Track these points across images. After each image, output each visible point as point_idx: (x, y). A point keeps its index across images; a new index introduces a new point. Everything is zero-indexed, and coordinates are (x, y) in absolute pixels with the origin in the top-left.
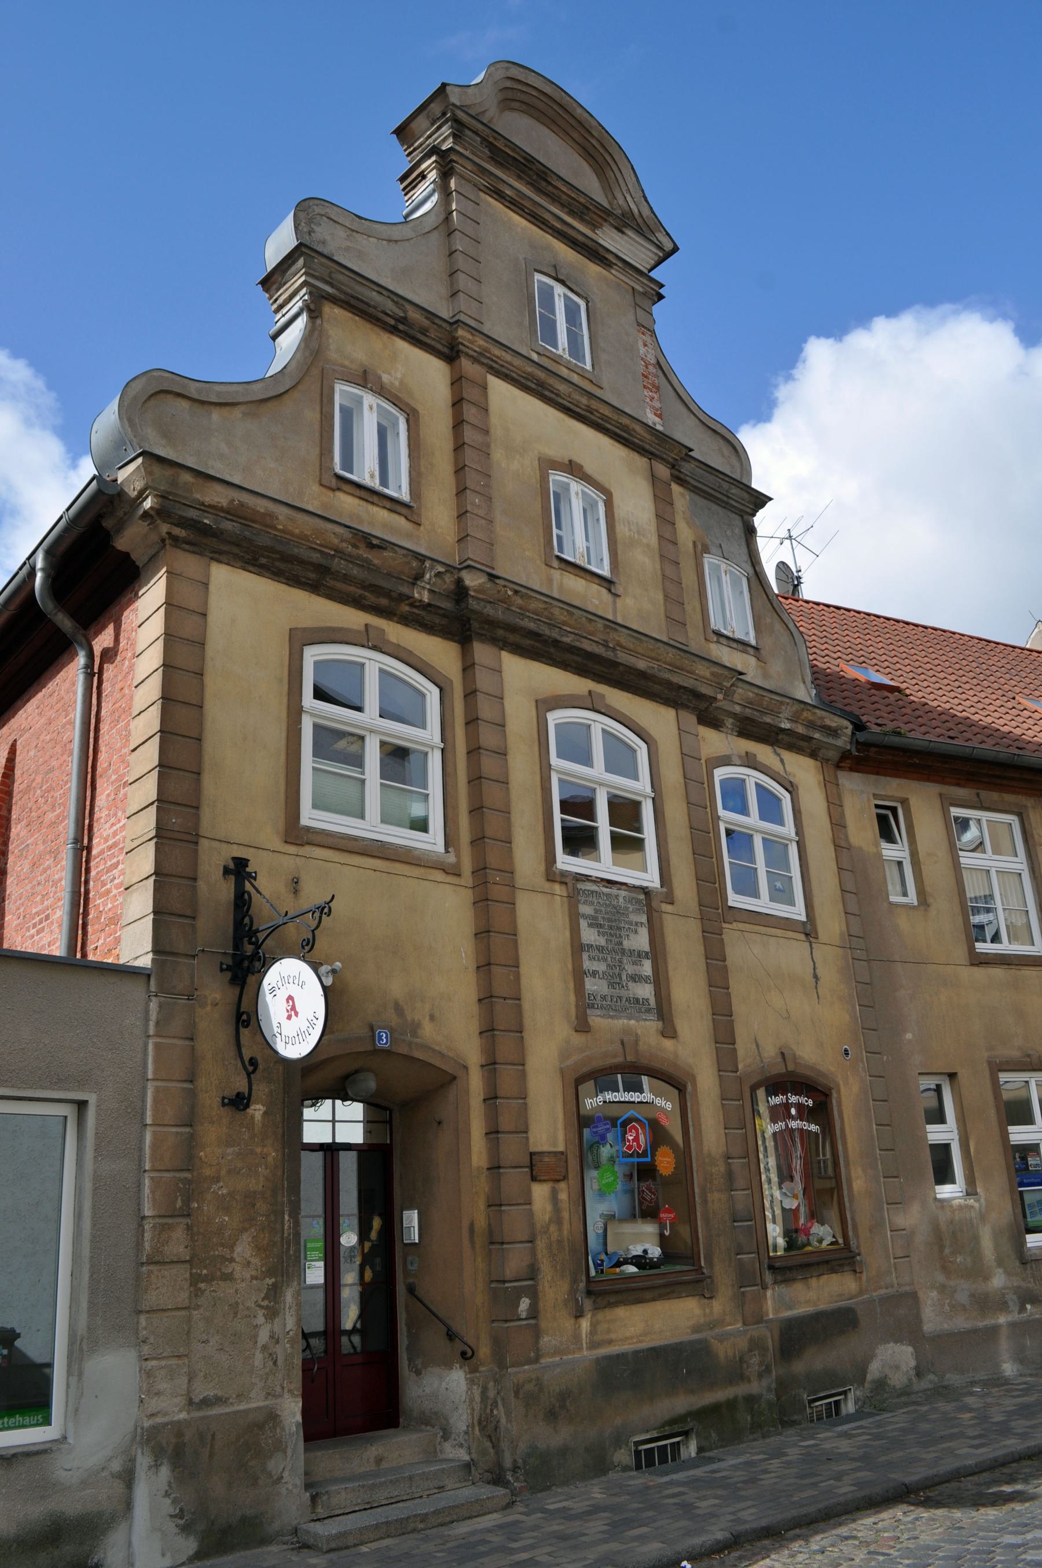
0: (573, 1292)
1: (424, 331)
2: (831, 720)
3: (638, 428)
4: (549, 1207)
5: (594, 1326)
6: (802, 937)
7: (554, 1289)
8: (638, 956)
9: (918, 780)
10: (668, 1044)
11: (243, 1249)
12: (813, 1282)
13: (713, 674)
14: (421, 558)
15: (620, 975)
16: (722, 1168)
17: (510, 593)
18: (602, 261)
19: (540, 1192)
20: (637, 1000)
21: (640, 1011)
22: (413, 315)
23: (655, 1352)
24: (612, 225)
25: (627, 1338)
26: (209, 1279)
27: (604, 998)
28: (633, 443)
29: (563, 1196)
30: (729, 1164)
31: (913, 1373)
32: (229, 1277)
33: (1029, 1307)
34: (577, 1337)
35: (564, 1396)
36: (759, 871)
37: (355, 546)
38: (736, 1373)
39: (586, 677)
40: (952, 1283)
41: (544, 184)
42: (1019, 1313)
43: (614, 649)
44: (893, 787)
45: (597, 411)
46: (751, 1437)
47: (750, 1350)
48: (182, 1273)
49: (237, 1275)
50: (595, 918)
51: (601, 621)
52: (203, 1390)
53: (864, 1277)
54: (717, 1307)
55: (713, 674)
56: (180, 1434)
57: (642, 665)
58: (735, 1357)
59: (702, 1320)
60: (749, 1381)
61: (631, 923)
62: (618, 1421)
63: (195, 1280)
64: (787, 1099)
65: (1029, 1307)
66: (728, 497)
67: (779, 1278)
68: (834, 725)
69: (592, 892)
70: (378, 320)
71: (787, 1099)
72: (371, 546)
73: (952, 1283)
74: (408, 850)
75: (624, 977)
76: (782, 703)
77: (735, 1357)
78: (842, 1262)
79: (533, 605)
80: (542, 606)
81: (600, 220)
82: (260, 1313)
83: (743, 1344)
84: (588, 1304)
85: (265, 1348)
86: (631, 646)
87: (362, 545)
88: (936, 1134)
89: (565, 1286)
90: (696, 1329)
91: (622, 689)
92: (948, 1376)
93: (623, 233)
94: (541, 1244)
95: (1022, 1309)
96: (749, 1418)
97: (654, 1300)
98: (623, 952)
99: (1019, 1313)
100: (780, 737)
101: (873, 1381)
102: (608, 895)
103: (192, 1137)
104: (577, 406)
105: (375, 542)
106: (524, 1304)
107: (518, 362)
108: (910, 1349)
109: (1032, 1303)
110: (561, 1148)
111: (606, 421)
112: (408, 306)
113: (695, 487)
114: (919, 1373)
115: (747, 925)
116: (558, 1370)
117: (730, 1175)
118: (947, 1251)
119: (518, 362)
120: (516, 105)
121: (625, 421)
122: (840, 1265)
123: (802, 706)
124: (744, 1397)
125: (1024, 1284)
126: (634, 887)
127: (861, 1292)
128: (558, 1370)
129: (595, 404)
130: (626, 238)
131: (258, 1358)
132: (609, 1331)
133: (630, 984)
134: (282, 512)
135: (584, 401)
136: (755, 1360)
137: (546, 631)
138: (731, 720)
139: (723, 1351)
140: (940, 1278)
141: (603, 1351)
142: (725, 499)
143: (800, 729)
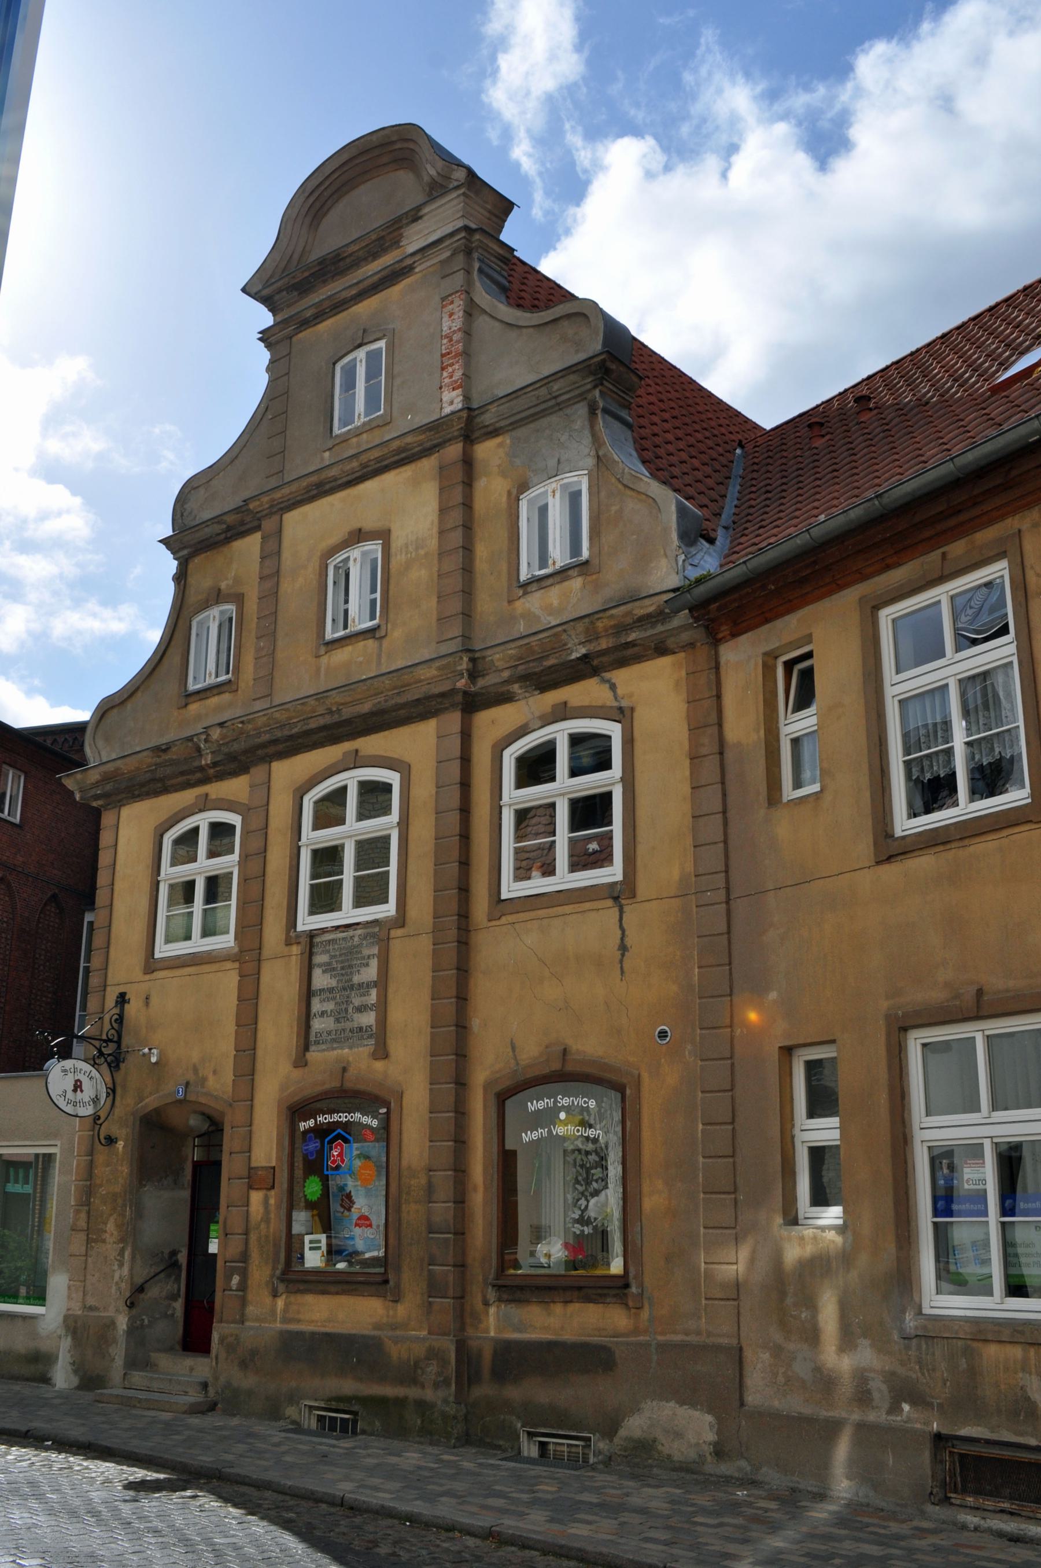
0: (272, 1276)
1: (242, 523)
2: (642, 608)
3: (409, 439)
4: (261, 1210)
5: (287, 1305)
6: (609, 903)
7: (260, 1272)
8: (364, 988)
9: (830, 593)
10: (379, 1065)
11: (110, 1226)
12: (558, 1308)
13: (439, 669)
14: (190, 739)
15: (346, 1010)
16: (423, 1181)
17: (240, 725)
18: (404, 274)
19: (256, 1197)
20: (361, 1029)
21: (362, 1038)
22: (230, 519)
23: (330, 1338)
24: (408, 224)
25: (313, 1321)
26: (96, 1241)
27: (329, 1033)
28: (413, 455)
29: (272, 1201)
30: (430, 1177)
31: (708, 1449)
32: (104, 1241)
33: (906, 1407)
34: (273, 1312)
35: (254, 1353)
36: (187, 943)
37: (159, 757)
38: (410, 1374)
39: (342, 742)
40: (791, 1346)
41: (341, 264)
42: (890, 1412)
43: (339, 710)
44: (785, 631)
45: (370, 461)
46: (418, 1439)
47: (427, 1358)
48: (82, 1236)
49: (108, 1241)
50: (329, 964)
51: (309, 699)
52: (91, 1301)
53: (645, 1314)
54: (401, 1310)
55: (439, 669)
56: (76, 1322)
57: (366, 707)
58: (409, 1359)
59: (385, 1320)
60: (423, 1387)
61: (363, 958)
62: (293, 1384)
63: (88, 1241)
64: (556, 1102)
65: (906, 1407)
66: (555, 397)
67: (505, 1296)
68: (651, 609)
69: (329, 941)
70: (216, 543)
71: (556, 1102)
72: (165, 751)
73: (791, 1346)
74: (209, 953)
75: (350, 1010)
76: (555, 635)
77: (409, 1359)
78: (605, 1291)
79: (261, 721)
80: (265, 718)
81: (396, 234)
82: (116, 1263)
83: (419, 1350)
84: (281, 1287)
85: (117, 1283)
86: (349, 699)
87: (161, 754)
88: (825, 1131)
89: (267, 1271)
90: (378, 1326)
91: (377, 732)
92: (764, 1469)
93: (420, 218)
94: (253, 1237)
95: (895, 1408)
96: (419, 1422)
97: (337, 1293)
98: (352, 988)
99: (890, 1412)
100: (595, 662)
101: (627, 1439)
102: (344, 939)
103: (92, 1161)
104: (353, 473)
105: (164, 747)
106: (236, 1280)
107: (294, 487)
108: (709, 1418)
109: (913, 1403)
110: (274, 1164)
111: (382, 461)
112: (225, 518)
113: (511, 424)
114: (720, 1452)
115: (522, 915)
116: (252, 1332)
117: (430, 1188)
118: (789, 1300)
119: (294, 487)
120: (329, 203)
121: (395, 445)
122: (600, 1295)
123: (587, 620)
124: (415, 1401)
125: (901, 1371)
126: (367, 922)
127: (636, 1331)
128: (252, 1332)
129: (364, 458)
130: (425, 218)
131: (114, 1289)
132: (299, 1312)
133: (355, 1015)
134: (119, 763)
135: (355, 464)
136: (433, 1368)
137: (279, 734)
138: (516, 686)
139: (396, 1352)
140: (778, 1337)
141: (293, 1327)
142: (553, 402)
143: (604, 644)
